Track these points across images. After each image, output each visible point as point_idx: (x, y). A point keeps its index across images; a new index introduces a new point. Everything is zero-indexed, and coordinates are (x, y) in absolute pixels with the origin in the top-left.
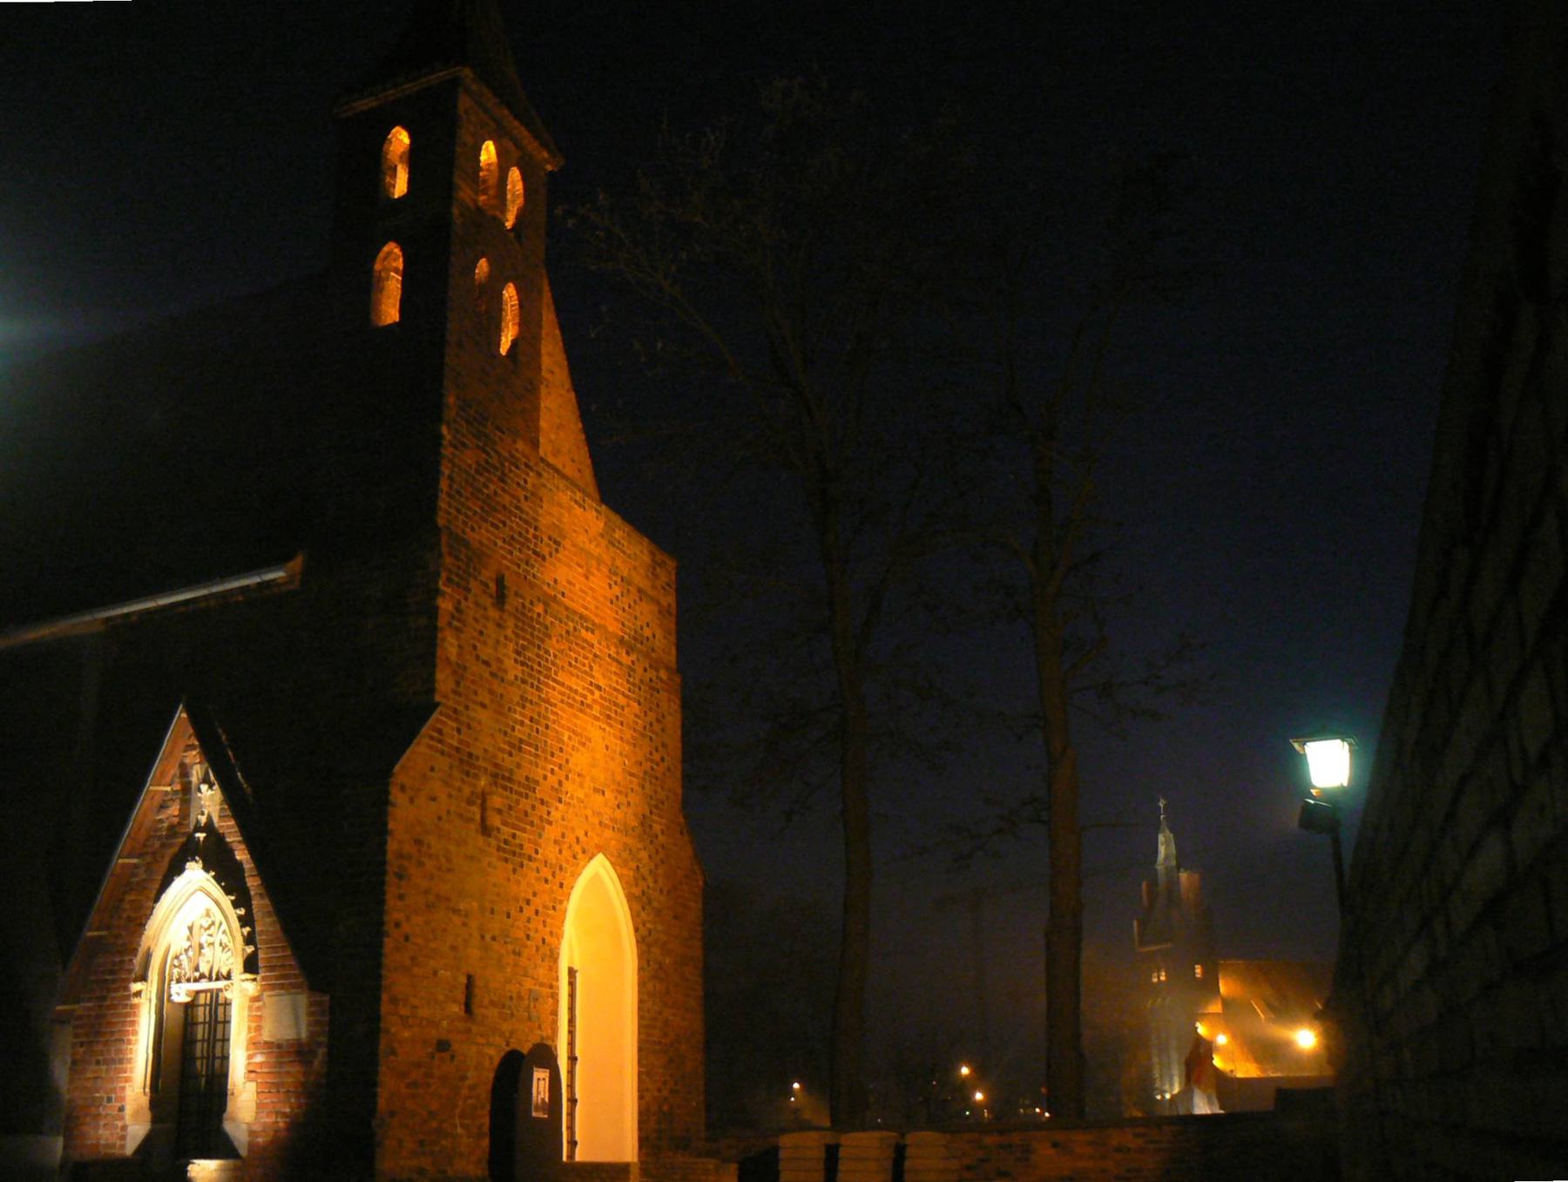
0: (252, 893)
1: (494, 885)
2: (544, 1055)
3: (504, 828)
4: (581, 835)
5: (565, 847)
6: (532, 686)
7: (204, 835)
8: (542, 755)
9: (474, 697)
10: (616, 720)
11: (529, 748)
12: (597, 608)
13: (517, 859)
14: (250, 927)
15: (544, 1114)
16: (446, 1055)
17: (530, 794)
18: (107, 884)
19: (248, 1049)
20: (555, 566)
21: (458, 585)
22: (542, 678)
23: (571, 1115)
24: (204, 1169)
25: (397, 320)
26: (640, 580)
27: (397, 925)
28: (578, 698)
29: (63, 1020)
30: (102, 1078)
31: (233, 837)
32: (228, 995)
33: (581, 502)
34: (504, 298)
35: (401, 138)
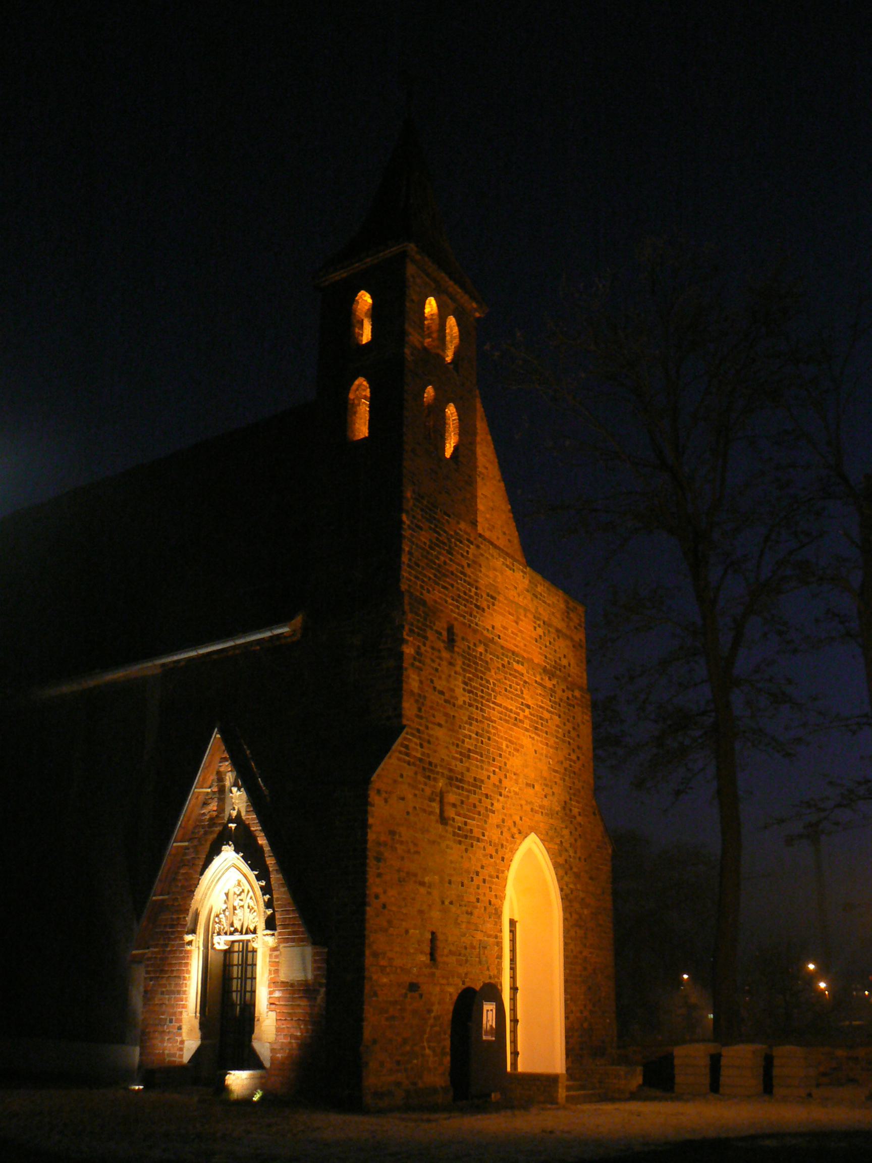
0: (271, 869)
1: (451, 862)
2: (492, 992)
3: (458, 817)
4: (517, 819)
5: (505, 830)
6: (477, 708)
7: (235, 825)
8: (486, 760)
9: (432, 719)
10: (542, 730)
11: (476, 756)
12: (525, 645)
13: (469, 841)
14: (270, 895)
15: (492, 1037)
16: (416, 994)
17: (477, 790)
18: (167, 861)
19: (269, 987)
20: (492, 615)
21: (419, 635)
22: (484, 702)
23: (514, 1031)
24: (238, 1078)
25: (367, 435)
26: (558, 623)
27: (377, 897)
28: (513, 715)
29: (138, 960)
30: (165, 1004)
31: (256, 828)
32: (255, 945)
33: (511, 566)
34: (447, 415)
35: (365, 299)
